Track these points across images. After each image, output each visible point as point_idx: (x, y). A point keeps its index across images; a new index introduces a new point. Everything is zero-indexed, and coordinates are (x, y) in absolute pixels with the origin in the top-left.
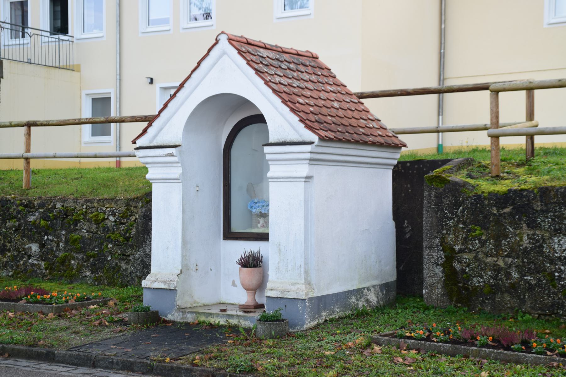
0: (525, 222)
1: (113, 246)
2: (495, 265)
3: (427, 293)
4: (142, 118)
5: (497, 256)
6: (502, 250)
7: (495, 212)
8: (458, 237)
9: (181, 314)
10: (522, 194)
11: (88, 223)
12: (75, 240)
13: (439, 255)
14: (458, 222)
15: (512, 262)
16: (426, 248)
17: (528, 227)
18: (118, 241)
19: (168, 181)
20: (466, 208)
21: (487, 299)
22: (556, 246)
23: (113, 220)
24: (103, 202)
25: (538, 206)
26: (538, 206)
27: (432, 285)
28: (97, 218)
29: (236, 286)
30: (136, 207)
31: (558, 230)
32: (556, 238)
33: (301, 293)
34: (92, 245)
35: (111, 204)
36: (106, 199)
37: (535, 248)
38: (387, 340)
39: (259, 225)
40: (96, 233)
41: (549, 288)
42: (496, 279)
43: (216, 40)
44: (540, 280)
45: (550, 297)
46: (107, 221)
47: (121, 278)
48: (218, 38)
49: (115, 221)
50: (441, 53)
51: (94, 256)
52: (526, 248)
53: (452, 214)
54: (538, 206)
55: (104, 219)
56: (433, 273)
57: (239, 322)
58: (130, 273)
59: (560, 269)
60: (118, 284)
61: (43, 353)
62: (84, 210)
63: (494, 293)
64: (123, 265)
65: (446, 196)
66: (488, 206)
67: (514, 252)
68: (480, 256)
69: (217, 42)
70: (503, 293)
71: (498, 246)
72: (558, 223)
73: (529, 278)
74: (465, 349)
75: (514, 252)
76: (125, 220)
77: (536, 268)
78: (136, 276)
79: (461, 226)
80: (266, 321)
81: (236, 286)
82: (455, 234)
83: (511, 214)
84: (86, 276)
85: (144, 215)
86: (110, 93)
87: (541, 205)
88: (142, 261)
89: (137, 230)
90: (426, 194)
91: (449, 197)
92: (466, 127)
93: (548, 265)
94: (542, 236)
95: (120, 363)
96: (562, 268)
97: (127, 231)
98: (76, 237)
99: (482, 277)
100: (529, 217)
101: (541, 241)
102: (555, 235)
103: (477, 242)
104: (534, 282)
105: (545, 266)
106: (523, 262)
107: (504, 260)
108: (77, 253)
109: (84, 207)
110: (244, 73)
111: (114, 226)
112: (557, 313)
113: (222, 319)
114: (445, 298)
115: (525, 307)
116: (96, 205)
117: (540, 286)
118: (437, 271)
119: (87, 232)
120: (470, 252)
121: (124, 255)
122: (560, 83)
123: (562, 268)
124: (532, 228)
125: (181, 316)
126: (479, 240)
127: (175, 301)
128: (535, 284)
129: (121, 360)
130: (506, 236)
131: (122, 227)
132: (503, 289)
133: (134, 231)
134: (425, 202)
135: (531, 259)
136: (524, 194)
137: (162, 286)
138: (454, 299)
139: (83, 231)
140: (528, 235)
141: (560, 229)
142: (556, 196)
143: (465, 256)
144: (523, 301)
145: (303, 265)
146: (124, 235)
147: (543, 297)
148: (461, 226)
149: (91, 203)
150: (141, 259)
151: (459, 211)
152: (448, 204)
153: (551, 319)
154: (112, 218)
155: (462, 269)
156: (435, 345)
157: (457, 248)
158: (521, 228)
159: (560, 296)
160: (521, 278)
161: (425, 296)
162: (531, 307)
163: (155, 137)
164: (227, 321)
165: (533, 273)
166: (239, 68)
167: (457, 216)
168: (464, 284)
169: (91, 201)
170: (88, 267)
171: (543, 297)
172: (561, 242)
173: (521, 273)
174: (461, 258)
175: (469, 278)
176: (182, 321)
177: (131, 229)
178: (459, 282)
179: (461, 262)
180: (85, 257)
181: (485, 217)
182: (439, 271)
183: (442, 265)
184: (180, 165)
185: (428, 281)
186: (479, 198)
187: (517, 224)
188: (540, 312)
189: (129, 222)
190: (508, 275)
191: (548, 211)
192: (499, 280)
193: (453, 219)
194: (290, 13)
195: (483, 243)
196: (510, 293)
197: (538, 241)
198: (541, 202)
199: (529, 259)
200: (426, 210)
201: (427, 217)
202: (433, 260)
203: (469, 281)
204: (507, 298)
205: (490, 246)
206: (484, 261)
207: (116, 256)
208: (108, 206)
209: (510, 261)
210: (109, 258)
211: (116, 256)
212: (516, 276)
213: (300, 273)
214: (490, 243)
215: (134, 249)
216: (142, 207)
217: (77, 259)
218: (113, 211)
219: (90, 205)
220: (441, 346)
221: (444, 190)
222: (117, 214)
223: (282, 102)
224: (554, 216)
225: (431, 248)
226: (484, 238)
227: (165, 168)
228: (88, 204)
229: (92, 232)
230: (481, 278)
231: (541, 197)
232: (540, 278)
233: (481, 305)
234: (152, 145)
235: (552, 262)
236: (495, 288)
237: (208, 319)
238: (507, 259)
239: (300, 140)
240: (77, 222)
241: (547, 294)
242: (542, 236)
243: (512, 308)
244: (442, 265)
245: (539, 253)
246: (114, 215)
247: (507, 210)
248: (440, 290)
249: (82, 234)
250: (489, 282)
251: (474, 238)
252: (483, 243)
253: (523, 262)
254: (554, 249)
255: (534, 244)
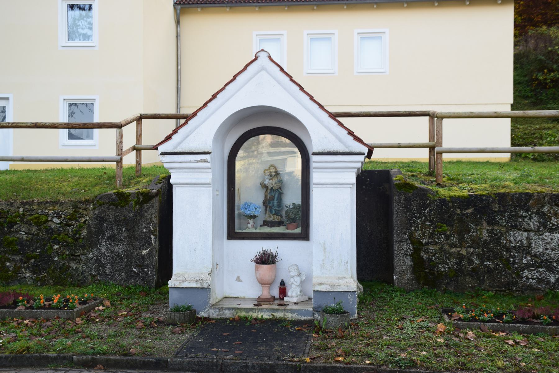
0: (485, 220)
1: (60, 247)
2: (459, 254)
3: (397, 279)
4: (80, 125)
5: (460, 247)
6: (465, 242)
7: (458, 213)
8: (425, 233)
9: (217, 310)
10: (482, 199)
11: (26, 226)
12: (12, 242)
13: (408, 247)
14: (426, 220)
15: (474, 251)
16: (396, 242)
17: (488, 224)
18: (66, 242)
19: (196, 186)
20: (433, 209)
21: (451, 281)
22: (512, 238)
23: (59, 222)
24: (45, 204)
25: (496, 208)
26: (496, 208)
27: (402, 272)
28: (39, 220)
29: (241, 281)
30: (85, 209)
31: (514, 226)
32: (511, 232)
33: (352, 286)
34: (33, 246)
35: (54, 207)
36: (47, 202)
37: (494, 240)
38: (467, 324)
39: (250, 226)
40: (38, 234)
41: (505, 271)
42: (460, 265)
43: (255, 56)
44: (497, 264)
45: (506, 277)
46: (50, 223)
47: (71, 278)
48: (258, 55)
49: (61, 223)
50: (178, 87)
51: (35, 258)
52: (486, 240)
53: (421, 214)
54: (495, 208)
55: (47, 221)
56: (403, 261)
57: (285, 315)
58: (82, 273)
59: (514, 255)
60: (68, 283)
61: (151, 362)
62: (21, 213)
63: (458, 276)
64: (73, 265)
65: (415, 200)
66: (452, 207)
67: (475, 243)
68: (445, 247)
69: (256, 58)
70: (465, 275)
71: (461, 239)
72: (514, 221)
73: (488, 263)
74: (543, 328)
75: (475, 243)
76: (74, 222)
77: (495, 255)
78: (90, 275)
79: (428, 223)
80: (337, 314)
81: (241, 281)
82: (422, 230)
83: (472, 214)
84: (25, 277)
85: (97, 217)
86: (8, 99)
87: (499, 207)
88: (96, 260)
89: (89, 231)
90: (396, 198)
91: (417, 201)
92: (382, 145)
93: (505, 253)
94: (500, 231)
95: (257, 366)
96: (516, 254)
97: (77, 232)
98: (11, 239)
99: (447, 264)
100: (489, 216)
101: (499, 234)
102: (511, 230)
103: (443, 236)
104: (492, 266)
105: (501, 253)
106: (483, 251)
107: (466, 250)
108: (13, 255)
109: (21, 209)
110: (285, 89)
111: (60, 227)
112: (512, 289)
113: (266, 313)
114: (414, 282)
115: (484, 286)
116: (35, 207)
117: (497, 269)
118: (406, 260)
119: (26, 234)
120: (436, 244)
121: (72, 255)
122: (495, 115)
123: (516, 254)
124: (492, 225)
125: (218, 313)
126: (445, 234)
127: (208, 298)
128: (494, 268)
129: (257, 364)
130: (468, 231)
131: (70, 229)
132: (466, 273)
133: (84, 232)
134: (395, 204)
135: (490, 248)
136: (484, 198)
137: (194, 285)
138: (421, 282)
139: (21, 233)
140: (487, 230)
141: (516, 225)
142: (512, 200)
143: (431, 248)
144: (483, 281)
145: (349, 261)
146: (73, 237)
147: (501, 277)
148: (428, 223)
149: (30, 206)
150: (95, 258)
151: (426, 212)
152: (416, 206)
153: (505, 294)
154: (56, 220)
155: (428, 258)
156: (514, 326)
157: (424, 241)
158: (482, 224)
159: (514, 276)
160: (482, 263)
161: (396, 281)
162: (489, 285)
163: (179, 143)
164: (272, 315)
165: (491, 260)
166: (279, 83)
167: (424, 216)
168: (430, 270)
169: (31, 204)
170: (29, 268)
171: (501, 277)
172: (516, 235)
173: (481, 259)
174: (427, 249)
175: (435, 265)
176: (219, 317)
177: (81, 231)
178: (425, 269)
179: (428, 253)
180: (24, 258)
181: (449, 217)
182: (408, 261)
183: (410, 255)
184: (210, 170)
185: (397, 269)
186: (443, 201)
187: (478, 222)
188: (497, 289)
189: (78, 223)
190: (470, 262)
191: (505, 211)
192: (463, 266)
193: (421, 218)
194: (71, 43)
195: (448, 237)
196: (470, 275)
197: (496, 234)
198: (499, 204)
199: (488, 248)
200: (396, 211)
201: (396, 217)
202: (402, 252)
203: (435, 267)
204: (468, 279)
205: (454, 239)
206: (449, 250)
207: (64, 256)
208: (51, 208)
209: (472, 251)
210: (56, 259)
211: (64, 256)
212: (477, 262)
213: (347, 269)
214: (454, 237)
215: (86, 249)
216: (94, 209)
217: (14, 260)
218: (58, 213)
219: (29, 207)
220: (520, 327)
221: (413, 195)
222: (63, 216)
223: (330, 116)
224: (510, 215)
225: (400, 242)
226: (448, 233)
227: (191, 173)
228: (26, 206)
229: (33, 234)
230: (446, 264)
231: (499, 200)
232: (497, 263)
233: (446, 286)
234: (176, 151)
235: (508, 250)
236: (459, 272)
237: (249, 314)
238: (469, 249)
239: (347, 150)
240: (11, 224)
241: (503, 275)
242: (500, 231)
243: (473, 287)
244: (410, 255)
245: (497, 244)
246: (59, 217)
247: (469, 211)
248: (409, 276)
249: (18, 236)
250: (453, 267)
251: (440, 233)
252: (448, 237)
253: (483, 251)
254: (510, 240)
255: (492, 237)
